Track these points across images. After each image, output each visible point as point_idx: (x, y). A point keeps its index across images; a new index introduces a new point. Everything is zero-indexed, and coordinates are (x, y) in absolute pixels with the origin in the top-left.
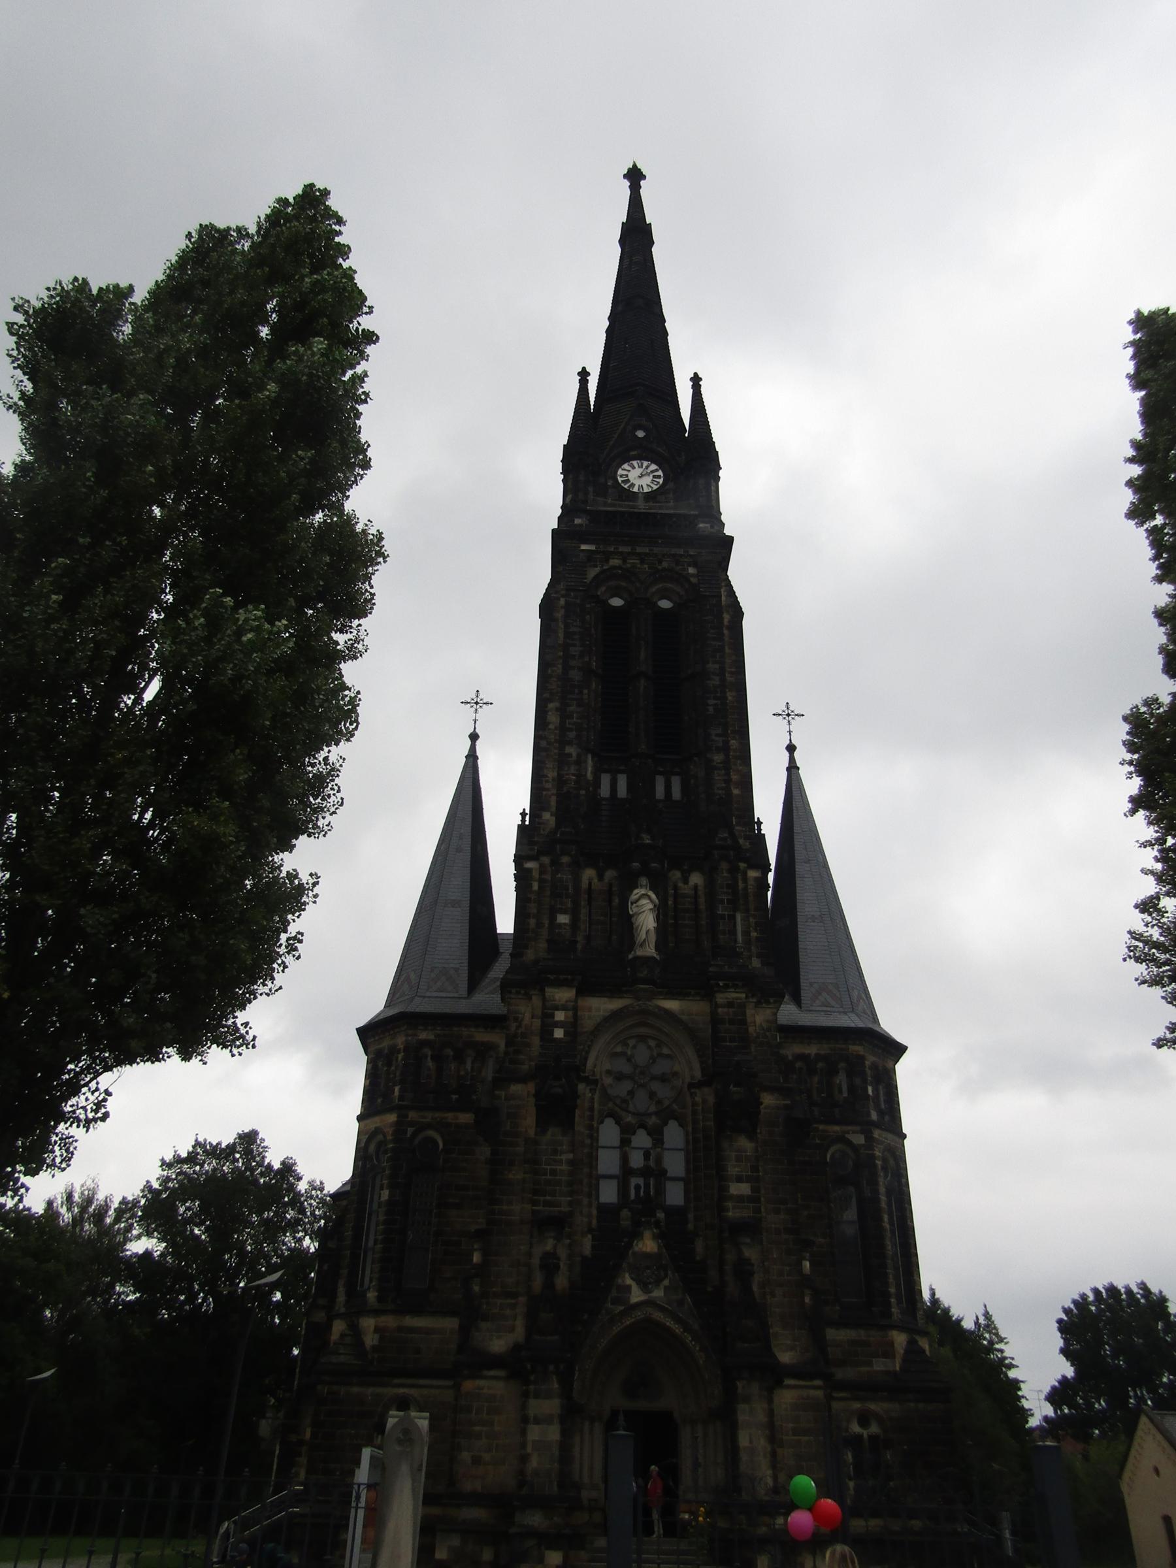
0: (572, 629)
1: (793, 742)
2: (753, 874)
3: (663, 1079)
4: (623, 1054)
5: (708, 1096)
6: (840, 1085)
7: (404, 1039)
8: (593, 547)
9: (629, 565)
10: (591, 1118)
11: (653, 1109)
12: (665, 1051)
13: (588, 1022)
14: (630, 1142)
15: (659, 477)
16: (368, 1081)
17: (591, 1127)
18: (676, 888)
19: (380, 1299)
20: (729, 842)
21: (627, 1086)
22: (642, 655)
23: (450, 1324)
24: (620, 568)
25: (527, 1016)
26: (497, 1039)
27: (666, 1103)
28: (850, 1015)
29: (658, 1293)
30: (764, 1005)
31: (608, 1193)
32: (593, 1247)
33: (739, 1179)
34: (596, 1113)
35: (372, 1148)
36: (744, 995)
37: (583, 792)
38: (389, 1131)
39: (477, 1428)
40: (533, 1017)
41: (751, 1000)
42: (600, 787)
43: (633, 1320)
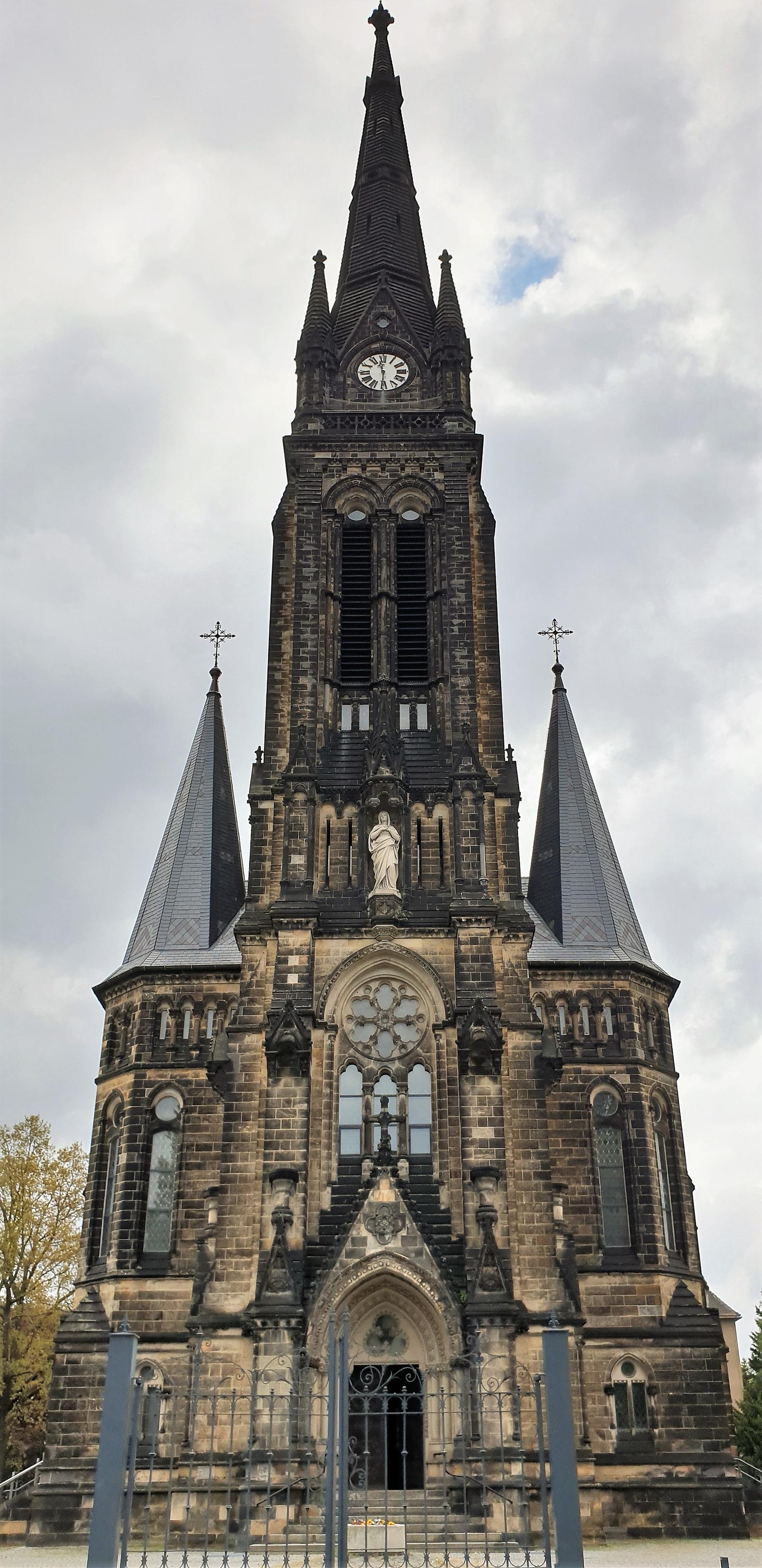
0: (306, 548)
1: (219, 667)
2: (501, 804)
3: (408, 1022)
4: (366, 998)
5: (451, 1035)
6: (605, 1022)
7: (141, 995)
8: (328, 455)
9: (369, 474)
10: (331, 1066)
11: (396, 1054)
12: (410, 993)
13: (325, 968)
14: (373, 1089)
15: (404, 372)
16: (106, 1042)
17: (330, 1076)
18: (419, 822)
19: (120, 1265)
20: (474, 771)
21: (371, 1030)
22: (384, 575)
23: (186, 1287)
24: (359, 477)
25: (263, 963)
26: (232, 988)
27: (410, 1047)
28: (616, 949)
29: (395, 1244)
30: (513, 941)
31: (351, 1145)
32: (334, 1201)
33: (482, 1123)
34: (335, 1061)
35: (111, 1112)
36: (488, 931)
37: (320, 726)
38: (127, 1093)
40: (268, 964)
41: (497, 935)
42: (340, 720)
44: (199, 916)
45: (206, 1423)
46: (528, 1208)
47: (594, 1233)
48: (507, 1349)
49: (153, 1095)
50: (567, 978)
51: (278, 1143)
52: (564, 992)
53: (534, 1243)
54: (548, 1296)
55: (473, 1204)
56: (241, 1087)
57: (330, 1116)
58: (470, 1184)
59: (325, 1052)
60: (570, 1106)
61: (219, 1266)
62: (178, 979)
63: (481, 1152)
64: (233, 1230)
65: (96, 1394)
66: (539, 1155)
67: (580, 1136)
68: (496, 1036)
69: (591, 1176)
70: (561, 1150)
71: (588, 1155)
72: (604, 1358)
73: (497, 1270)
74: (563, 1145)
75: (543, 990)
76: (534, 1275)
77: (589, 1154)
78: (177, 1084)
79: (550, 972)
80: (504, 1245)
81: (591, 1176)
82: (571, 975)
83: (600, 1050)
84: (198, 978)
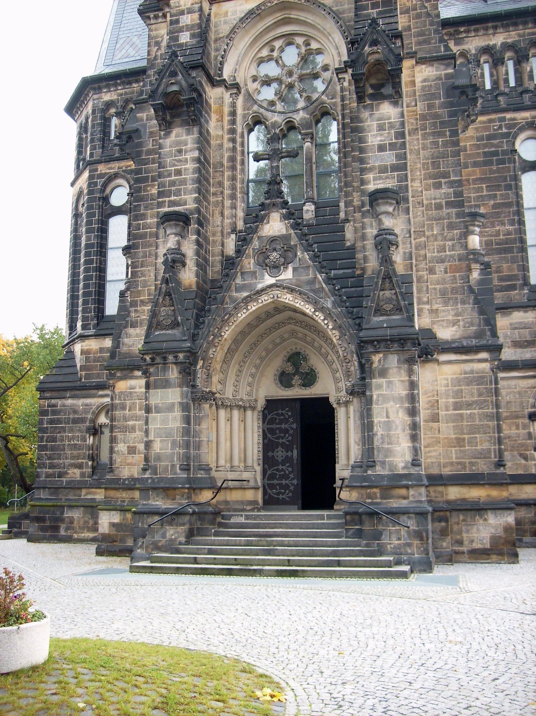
19: (84, 327)
39: (131, 423)
43: (260, 305)
44: (140, 33)
45: (126, 452)
46: (439, 238)
47: (519, 271)
48: (406, 373)
49: (105, 185)
50: (491, 31)
51: (170, 191)
52: (488, 46)
53: (446, 272)
54: (461, 323)
55: (371, 231)
56: (149, 152)
57: (233, 168)
58: (368, 211)
59: (226, 110)
60: (496, 154)
61: (133, 315)
62: (120, 85)
63: (380, 178)
64: (145, 281)
65: (71, 430)
66: (451, 184)
67: (505, 179)
68: (393, 53)
69: (516, 218)
70: (486, 196)
71: (512, 198)
72: (528, 388)
73: (396, 293)
74: (487, 191)
75: (466, 47)
76: (446, 304)
77: (515, 197)
78: (123, 174)
79: (473, 27)
80: (406, 270)
81: (516, 218)
82: (495, 28)
83: (526, 97)
84: (137, 81)
